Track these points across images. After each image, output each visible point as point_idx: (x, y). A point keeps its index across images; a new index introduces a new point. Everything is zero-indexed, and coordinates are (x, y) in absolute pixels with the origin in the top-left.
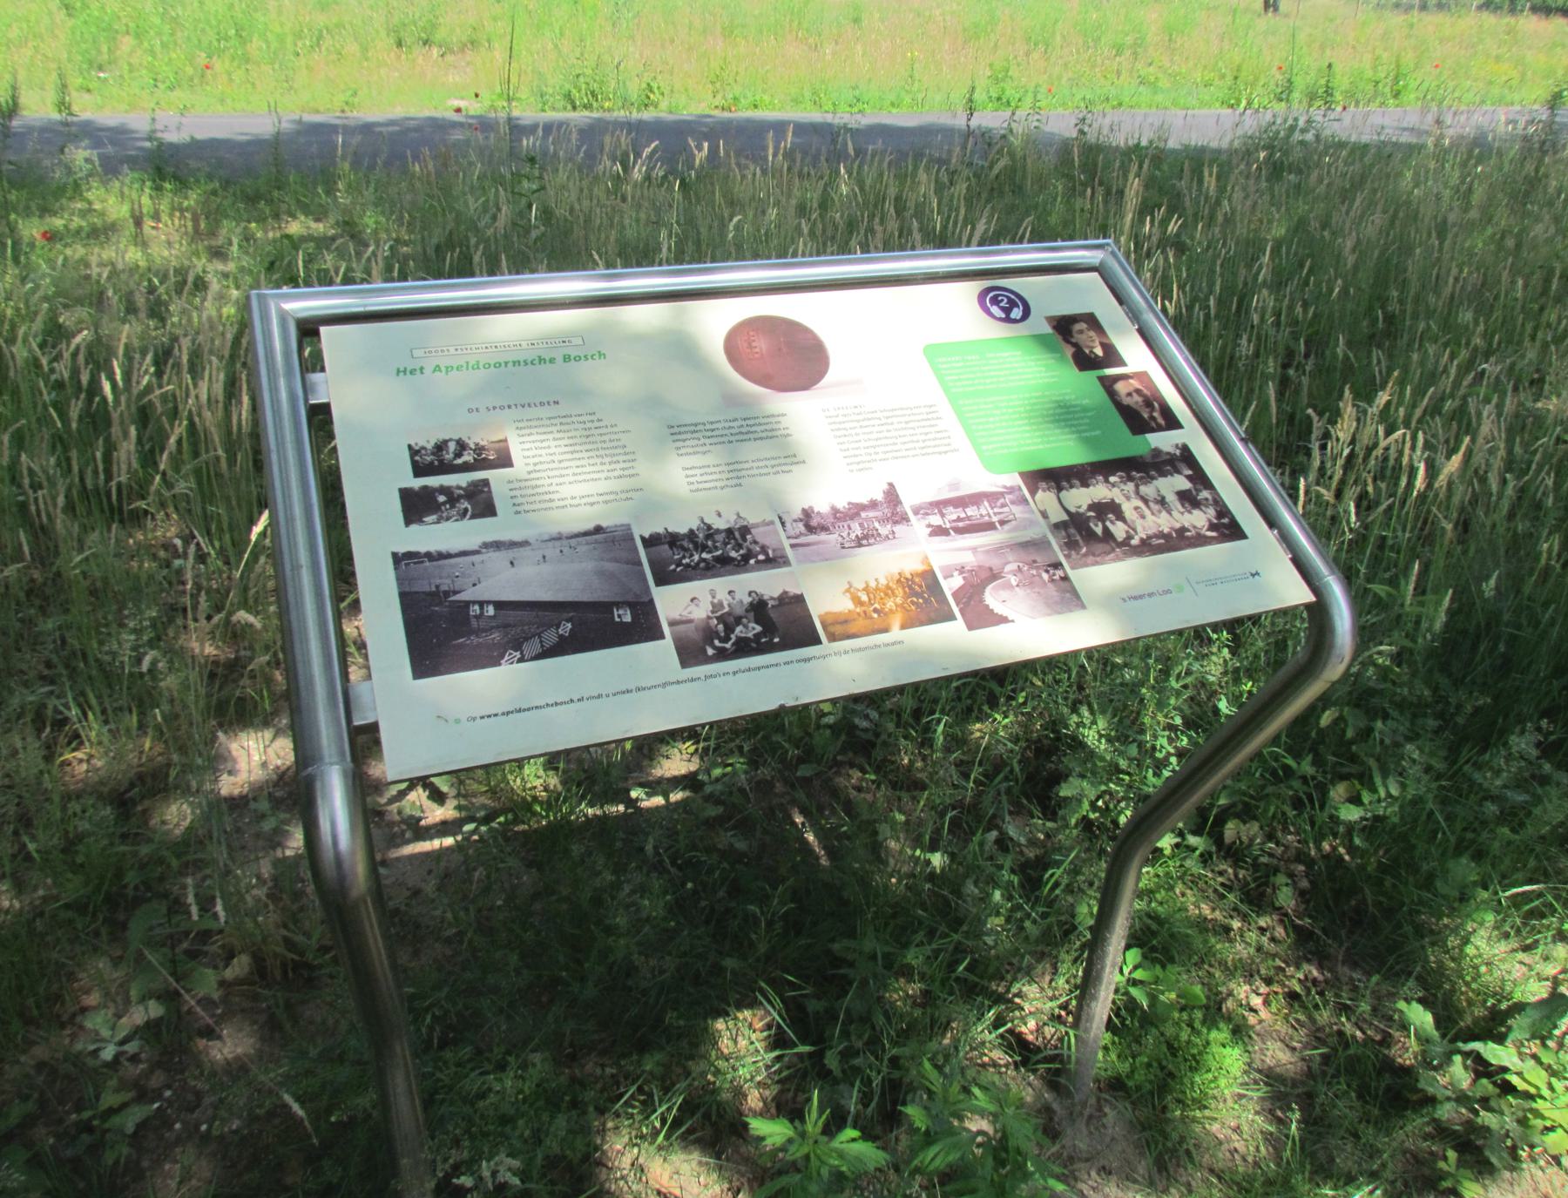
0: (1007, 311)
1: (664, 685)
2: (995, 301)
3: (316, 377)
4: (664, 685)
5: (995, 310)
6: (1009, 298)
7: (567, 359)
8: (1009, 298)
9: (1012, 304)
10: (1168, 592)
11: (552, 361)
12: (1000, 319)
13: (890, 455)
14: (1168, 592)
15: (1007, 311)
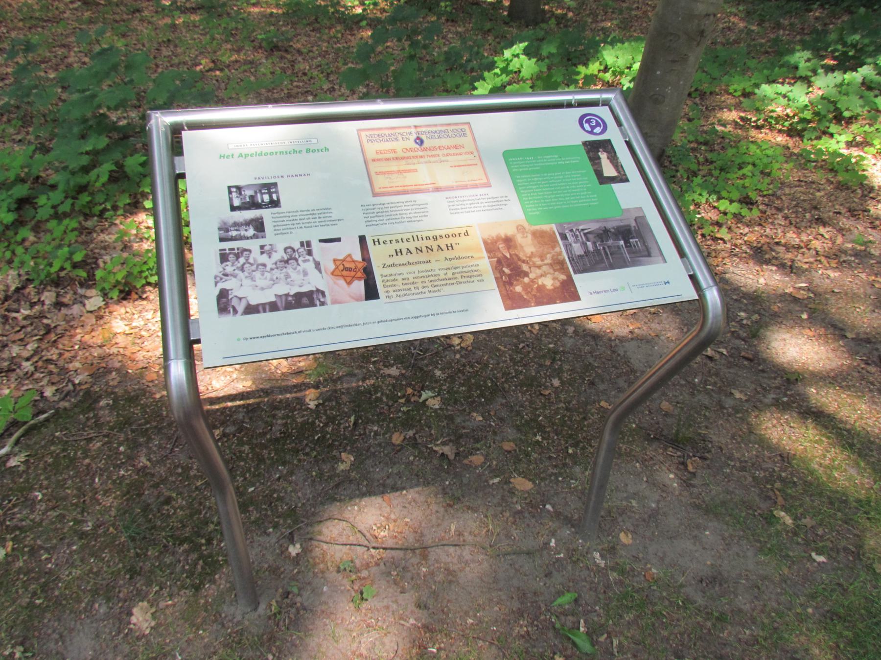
0: (593, 128)
1: (342, 327)
2: (588, 121)
3: (177, 159)
4: (342, 327)
5: (587, 126)
6: (597, 121)
7: (308, 151)
8: (597, 121)
9: (598, 125)
10: (616, 290)
11: (300, 152)
12: (587, 132)
13: (372, 207)
14: (616, 290)
15: (593, 128)
